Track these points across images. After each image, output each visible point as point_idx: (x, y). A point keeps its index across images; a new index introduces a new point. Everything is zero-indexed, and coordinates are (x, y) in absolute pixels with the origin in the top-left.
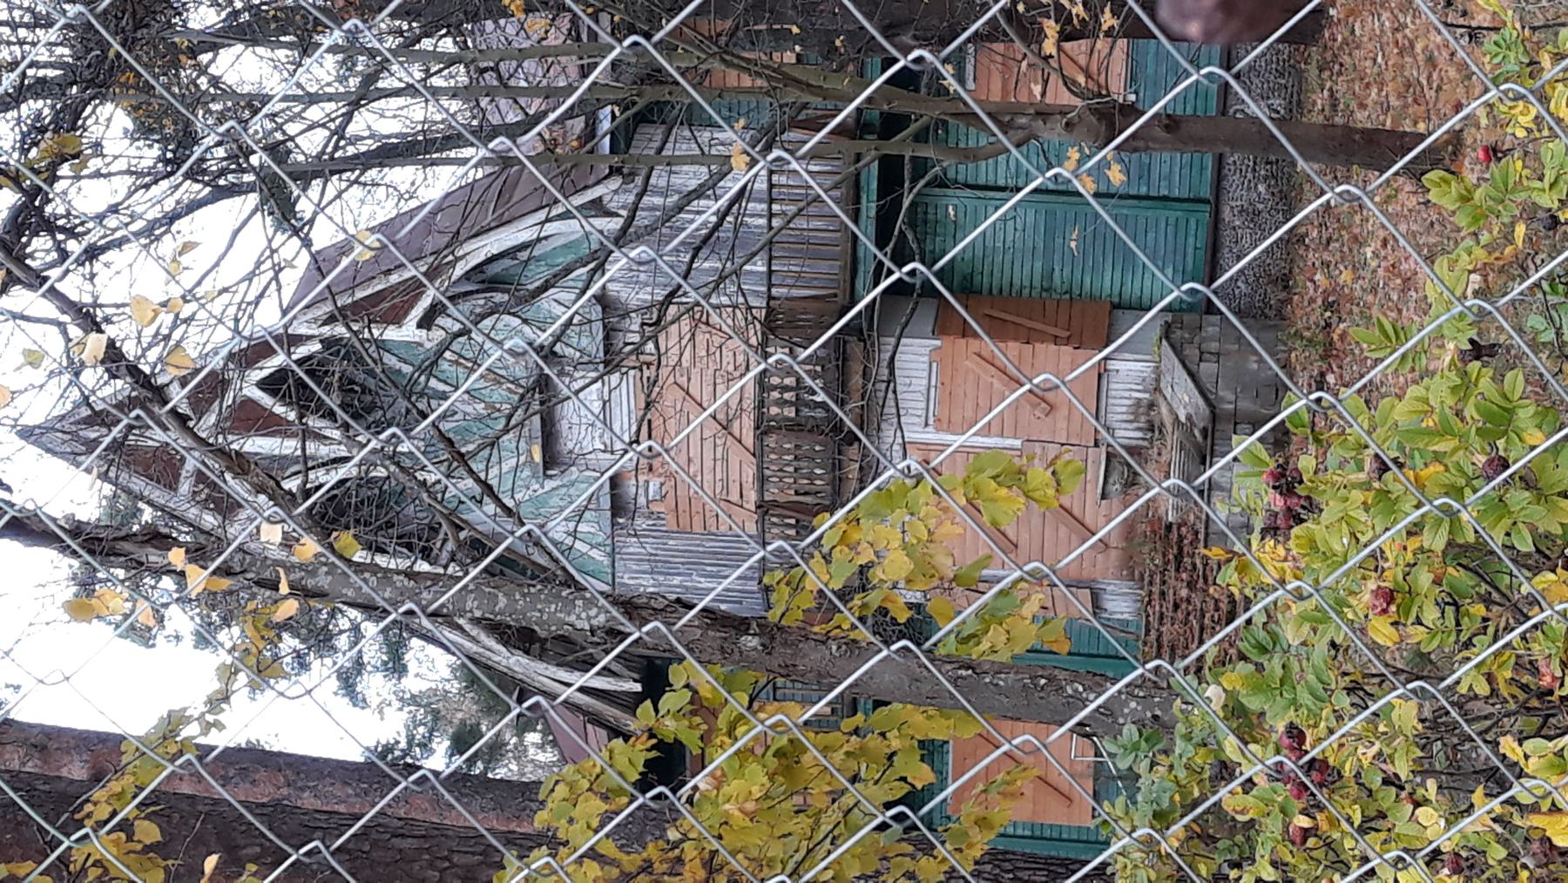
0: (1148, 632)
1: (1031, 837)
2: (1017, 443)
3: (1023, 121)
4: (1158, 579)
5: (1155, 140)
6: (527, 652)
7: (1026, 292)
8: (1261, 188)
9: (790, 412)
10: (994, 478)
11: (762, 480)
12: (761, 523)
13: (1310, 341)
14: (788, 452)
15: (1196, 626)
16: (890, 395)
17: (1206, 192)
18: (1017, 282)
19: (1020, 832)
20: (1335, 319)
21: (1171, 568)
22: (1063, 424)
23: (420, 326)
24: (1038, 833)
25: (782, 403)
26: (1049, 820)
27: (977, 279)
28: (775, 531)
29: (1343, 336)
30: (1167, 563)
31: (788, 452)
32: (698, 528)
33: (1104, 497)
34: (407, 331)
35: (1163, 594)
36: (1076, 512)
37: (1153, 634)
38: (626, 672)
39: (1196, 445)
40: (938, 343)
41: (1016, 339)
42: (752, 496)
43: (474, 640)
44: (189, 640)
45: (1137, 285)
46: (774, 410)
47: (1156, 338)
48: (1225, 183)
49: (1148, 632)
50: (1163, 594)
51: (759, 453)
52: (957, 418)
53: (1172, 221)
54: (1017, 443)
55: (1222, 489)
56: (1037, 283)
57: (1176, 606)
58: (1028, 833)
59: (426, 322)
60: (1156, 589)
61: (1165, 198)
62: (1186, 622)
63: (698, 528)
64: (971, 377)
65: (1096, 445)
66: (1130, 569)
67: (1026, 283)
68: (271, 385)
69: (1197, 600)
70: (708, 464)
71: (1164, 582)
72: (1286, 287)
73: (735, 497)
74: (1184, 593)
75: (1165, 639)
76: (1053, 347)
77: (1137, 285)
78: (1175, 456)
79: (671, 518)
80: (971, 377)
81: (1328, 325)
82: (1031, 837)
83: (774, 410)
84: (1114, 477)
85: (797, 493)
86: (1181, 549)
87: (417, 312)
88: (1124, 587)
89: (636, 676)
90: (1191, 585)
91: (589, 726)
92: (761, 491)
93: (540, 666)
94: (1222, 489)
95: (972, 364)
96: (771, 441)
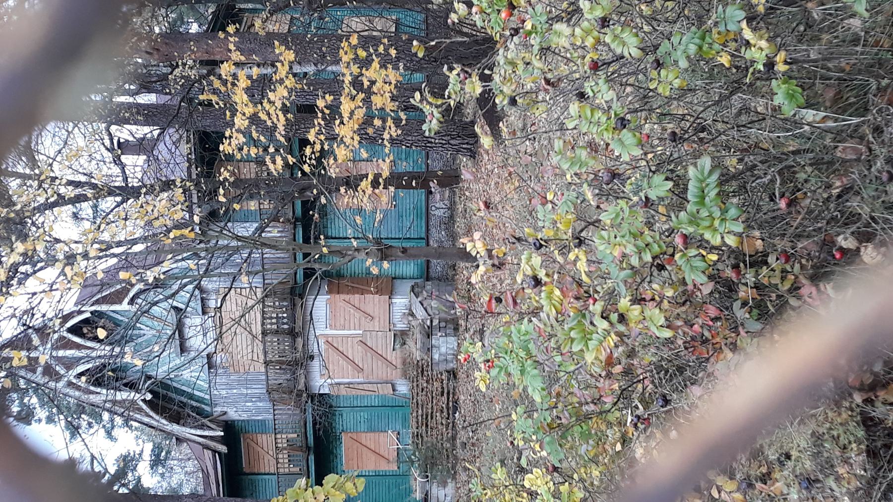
0: (413, 399)
1: (376, 476)
2: (361, 332)
3: (350, 253)
4: (415, 380)
5: (398, 256)
6: (178, 424)
7: (360, 275)
8: (443, 233)
9: (275, 327)
10: (333, 487)
11: (265, 353)
12: (266, 367)
13: (463, 297)
14: (275, 342)
15: (430, 397)
16: (311, 326)
17: (423, 235)
18: (357, 272)
19: (371, 474)
20: (471, 289)
21: (420, 375)
22: (377, 324)
23: (128, 304)
24: (377, 474)
25: (272, 324)
26: (382, 469)
27: (342, 272)
28: (272, 371)
29: (474, 295)
30: (418, 374)
31: (275, 342)
32: (242, 371)
33: (394, 350)
34: (124, 306)
35: (417, 385)
36: (384, 356)
37: (415, 401)
38: (218, 428)
39: (426, 332)
40: (329, 297)
41: (358, 293)
42: (262, 357)
43: (158, 421)
44: (44, 421)
45: (401, 269)
46: (269, 326)
47: (409, 292)
48: (430, 232)
49: (413, 399)
50: (417, 385)
51: (264, 342)
52: (338, 325)
53: (377, 482)
54: (361, 332)
55: (435, 347)
56: (364, 271)
57: (423, 389)
58: (374, 474)
59: (132, 302)
60: (415, 384)
61: (409, 238)
62: (427, 395)
63: (242, 371)
64: (342, 308)
65: (390, 330)
66: (405, 375)
67: (360, 272)
68: (71, 330)
69: (430, 387)
70: (245, 346)
71: (417, 381)
72: (454, 269)
73: (255, 358)
74: (425, 385)
75: (420, 402)
76: (371, 295)
77: (401, 269)
78: (419, 336)
79: (232, 368)
80: (342, 308)
81: (469, 290)
82: (376, 476)
83: (269, 326)
84: (397, 342)
85: (279, 357)
86: (423, 369)
87: (127, 300)
88: (404, 382)
89: (221, 429)
90: (427, 382)
91: (205, 450)
92: (265, 357)
93: (184, 429)
94: (435, 347)
95: (342, 304)
96: (268, 338)
